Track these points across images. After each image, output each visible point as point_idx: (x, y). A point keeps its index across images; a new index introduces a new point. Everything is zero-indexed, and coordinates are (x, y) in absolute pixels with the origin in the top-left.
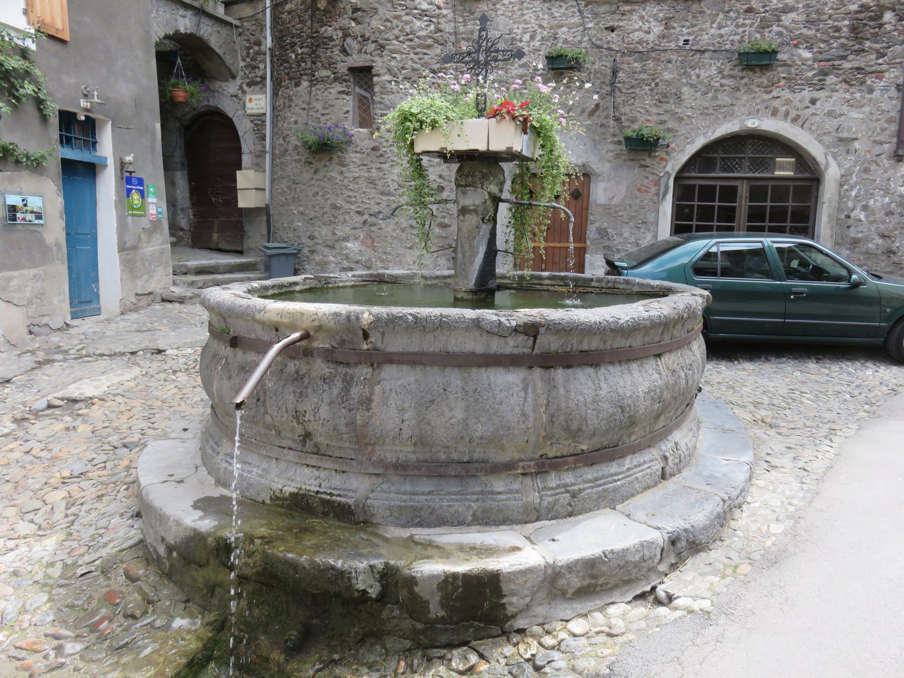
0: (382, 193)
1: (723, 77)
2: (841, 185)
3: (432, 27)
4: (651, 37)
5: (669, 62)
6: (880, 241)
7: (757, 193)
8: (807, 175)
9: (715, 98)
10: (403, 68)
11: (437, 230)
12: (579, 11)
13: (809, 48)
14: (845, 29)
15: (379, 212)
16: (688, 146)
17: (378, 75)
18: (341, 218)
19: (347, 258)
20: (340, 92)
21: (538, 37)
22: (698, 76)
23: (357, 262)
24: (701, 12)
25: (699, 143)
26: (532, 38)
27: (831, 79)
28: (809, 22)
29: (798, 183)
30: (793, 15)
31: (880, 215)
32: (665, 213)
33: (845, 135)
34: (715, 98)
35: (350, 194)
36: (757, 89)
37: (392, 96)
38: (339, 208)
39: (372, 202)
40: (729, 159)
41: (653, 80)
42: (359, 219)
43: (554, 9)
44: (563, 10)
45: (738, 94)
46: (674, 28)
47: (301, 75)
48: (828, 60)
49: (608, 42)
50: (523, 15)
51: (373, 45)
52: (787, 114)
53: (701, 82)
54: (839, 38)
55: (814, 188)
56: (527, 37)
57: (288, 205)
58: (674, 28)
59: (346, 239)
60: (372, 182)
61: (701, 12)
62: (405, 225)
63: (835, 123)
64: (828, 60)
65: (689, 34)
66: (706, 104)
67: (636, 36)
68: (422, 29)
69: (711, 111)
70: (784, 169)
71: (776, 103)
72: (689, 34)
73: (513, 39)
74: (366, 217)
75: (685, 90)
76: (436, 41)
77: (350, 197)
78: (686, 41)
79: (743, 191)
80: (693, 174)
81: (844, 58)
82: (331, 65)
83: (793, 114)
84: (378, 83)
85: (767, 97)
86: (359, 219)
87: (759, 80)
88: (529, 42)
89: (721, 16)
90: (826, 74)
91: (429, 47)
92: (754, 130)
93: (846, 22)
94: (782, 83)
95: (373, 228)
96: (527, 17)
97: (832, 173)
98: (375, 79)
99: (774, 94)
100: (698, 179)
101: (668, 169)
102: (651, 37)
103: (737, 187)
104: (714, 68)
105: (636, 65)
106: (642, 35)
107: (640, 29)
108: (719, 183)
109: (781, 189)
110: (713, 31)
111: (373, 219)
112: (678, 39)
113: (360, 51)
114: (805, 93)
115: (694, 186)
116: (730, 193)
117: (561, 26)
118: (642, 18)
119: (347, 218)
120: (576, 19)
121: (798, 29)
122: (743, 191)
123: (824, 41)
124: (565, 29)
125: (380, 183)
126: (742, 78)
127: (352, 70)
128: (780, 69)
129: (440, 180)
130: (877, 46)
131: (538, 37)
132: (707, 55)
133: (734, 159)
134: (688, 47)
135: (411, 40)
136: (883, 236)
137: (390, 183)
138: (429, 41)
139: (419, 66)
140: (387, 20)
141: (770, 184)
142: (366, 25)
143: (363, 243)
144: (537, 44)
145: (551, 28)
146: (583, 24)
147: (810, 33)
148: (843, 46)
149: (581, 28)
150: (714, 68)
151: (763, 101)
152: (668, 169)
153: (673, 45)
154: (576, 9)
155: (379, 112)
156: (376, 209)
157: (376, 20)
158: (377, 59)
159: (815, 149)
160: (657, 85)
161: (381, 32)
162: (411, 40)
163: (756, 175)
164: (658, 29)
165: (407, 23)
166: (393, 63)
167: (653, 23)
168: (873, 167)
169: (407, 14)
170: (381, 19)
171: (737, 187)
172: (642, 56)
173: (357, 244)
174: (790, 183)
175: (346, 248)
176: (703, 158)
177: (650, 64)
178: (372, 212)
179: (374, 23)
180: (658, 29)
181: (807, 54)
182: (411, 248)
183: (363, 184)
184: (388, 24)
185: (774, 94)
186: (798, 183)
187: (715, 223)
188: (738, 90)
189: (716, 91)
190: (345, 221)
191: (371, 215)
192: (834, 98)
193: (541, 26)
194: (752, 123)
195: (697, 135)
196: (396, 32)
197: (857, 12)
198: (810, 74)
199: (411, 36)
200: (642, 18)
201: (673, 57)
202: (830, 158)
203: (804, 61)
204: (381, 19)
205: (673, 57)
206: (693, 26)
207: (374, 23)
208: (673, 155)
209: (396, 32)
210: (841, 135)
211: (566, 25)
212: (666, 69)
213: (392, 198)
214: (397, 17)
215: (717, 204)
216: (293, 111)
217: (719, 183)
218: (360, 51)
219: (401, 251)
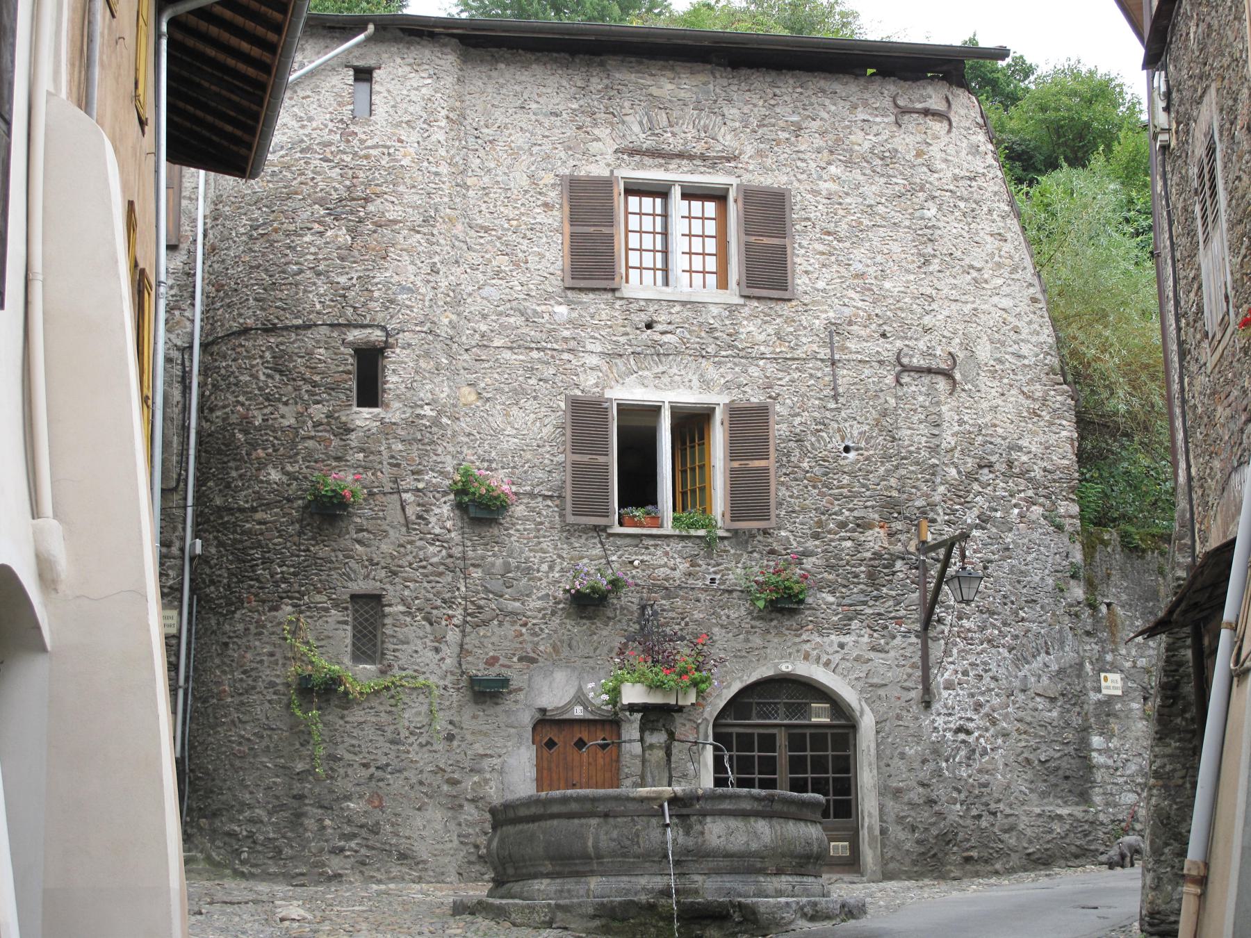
0: (392, 742)
1: (753, 619)
2: (878, 732)
3: (444, 553)
4: (677, 574)
5: (698, 601)
6: (921, 790)
7: (796, 741)
8: (843, 722)
9: (747, 640)
10: (417, 598)
11: (445, 788)
12: (601, 543)
13: (832, 592)
14: (863, 576)
15: (388, 765)
16: (725, 691)
17: (390, 605)
18: (342, 771)
19: (349, 821)
20: (339, 622)
21: (558, 568)
22: (728, 617)
23: (362, 826)
24: (725, 551)
25: (736, 687)
26: (551, 568)
27: (855, 624)
28: (830, 567)
29: (835, 731)
30: (814, 559)
31: (916, 765)
32: (706, 765)
33: (875, 680)
34: (747, 640)
35: (354, 742)
36: (787, 632)
37: (406, 629)
38: (340, 759)
39: (379, 752)
40: (764, 704)
41: (683, 619)
42: (365, 773)
43: (573, 540)
44: (583, 541)
45: (769, 637)
46: (700, 566)
47: (282, 598)
48: (851, 605)
49: (633, 577)
50: (540, 543)
51: (383, 571)
52: (818, 659)
53: (731, 624)
54: (859, 583)
55: (851, 736)
56: (545, 567)
57: (255, 756)
58: (700, 566)
59: (348, 798)
60: (380, 728)
61: (725, 551)
62: (414, 780)
63: (865, 668)
64: (851, 605)
65: (715, 573)
66: (739, 646)
67: (661, 572)
68: (435, 555)
69: (744, 654)
70: (820, 716)
71: (807, 647)
72: (715, 573)
73: (529, 568)
74: (372, 770)
75: (716, 630)
76: (448, 568)
77: (353, 746)
78: (713, 580)
79: (782, 740)
80: (729, 721)
81: (865, 603)
82: (327, 588)
83: (824, 658)
84: (390, 614)
85: (797, 640)
86: (365, 773)
87: (788, 623)
88: (547, 573)
89: (745, 556)
90: (851, 619)
91: (441, 574)
92: (788, 673)
93: (863, 569)
94: (810, 627)
95: (381, 784)
96: (544, 545)
97: (867, 723)
98: (387, 609)
99: (804, 637)
100: (736, 727)
101: (706, 715)
102: (677, 574)
103: (774, 735)
104: (743, 608)
105: (664, 602)
106: (669, 572)
107: (665, 565)
108: (756, 731)
109: (819, 736)
110: (739, 571)
111: (379, 774)
112: (704, 578)
113: (366, 577)
114: (833, 637)
115: (731, 734)
116: (768, 742)
117: (582, 558)
118: (666, 554)
119: (350, 771)
120: (598, 551)
121: (820, 573)
122: (782, 740)
123: (845, 586)
124: (585, 561)
125: (390, 729)
126: (771, 620)
127: (354, 597)
128: (807, 612)
129: (450, 727)
130: (893, 593)
131: (558, 568)
132: (735, 595)
133: (769, 704)
134: (715, 586)
135: (424, 567)
136: (923, 785)
137: (401, 730)
138: (442, 568)
139: (431, 596)
140: (402, 546)
141: (808, 731)
142: (374, 548)
143: (369, 801)
144: (557, 575)
145: (571, 559)
146: (606, 557)
147: (831, 577)
148: (862, 591)
149: (603, 561)
150: (743, 608)
151: (795, 644)
152: (706, 715)
153: (700, 584)
154: (597, 541)
155: (391, 647)
156: (384, 761)
157: (386, 544)
158: (388, 586)
159: (848, 694)
160: (687, 624)
161: (393, 557)
162: (424, 567)
163: (794, 722)
164: (684, 566)
165: (421, 548)
166: (406, 593)
167: (678, 560)
168: (904, 713)
169: (421, 539)
170: (393, 543)
171: (774, 735)
172: (669, 593)
173: (362, 803)
174: (829, 731)
175: (348, 808)
176: (738, 705)
177: (679, 602)
178: (379, 764)
179: (384, 547)
180: (684, 566)
181: (831, 599)
182: (419, 809)
183: (369, 732)
184: (402, 550)
185: (804, 637)
186: (835, 731)
187: (757, 776)
188: (769, 632)
189: (747, 632)
190: (347, 776)
191: (378, 768)
192: (858, 639)
193: (560, 556)
194: (786, 667)
195: (734, 679)
196: (410, 558)
197: (871, 559)
198: (835, 618)
199: (424, 563)
200: (666, 554)
201: (702, 596)
202: (863, 703)
203: (829, 604)
204: (393, 543)
205: (702, 596)
206: (718, 565)
207: (384, 547)
208: (709, 700)
209: (410, 558)
210: (870, 681)
211: (587, 557)
212: (695, 608)
213: (402, 748)
214: (411, 543)
215: (830, 753)
216: (265, 639)
217: (756, 731)
218: (366, 577)
219: (411, 813)
